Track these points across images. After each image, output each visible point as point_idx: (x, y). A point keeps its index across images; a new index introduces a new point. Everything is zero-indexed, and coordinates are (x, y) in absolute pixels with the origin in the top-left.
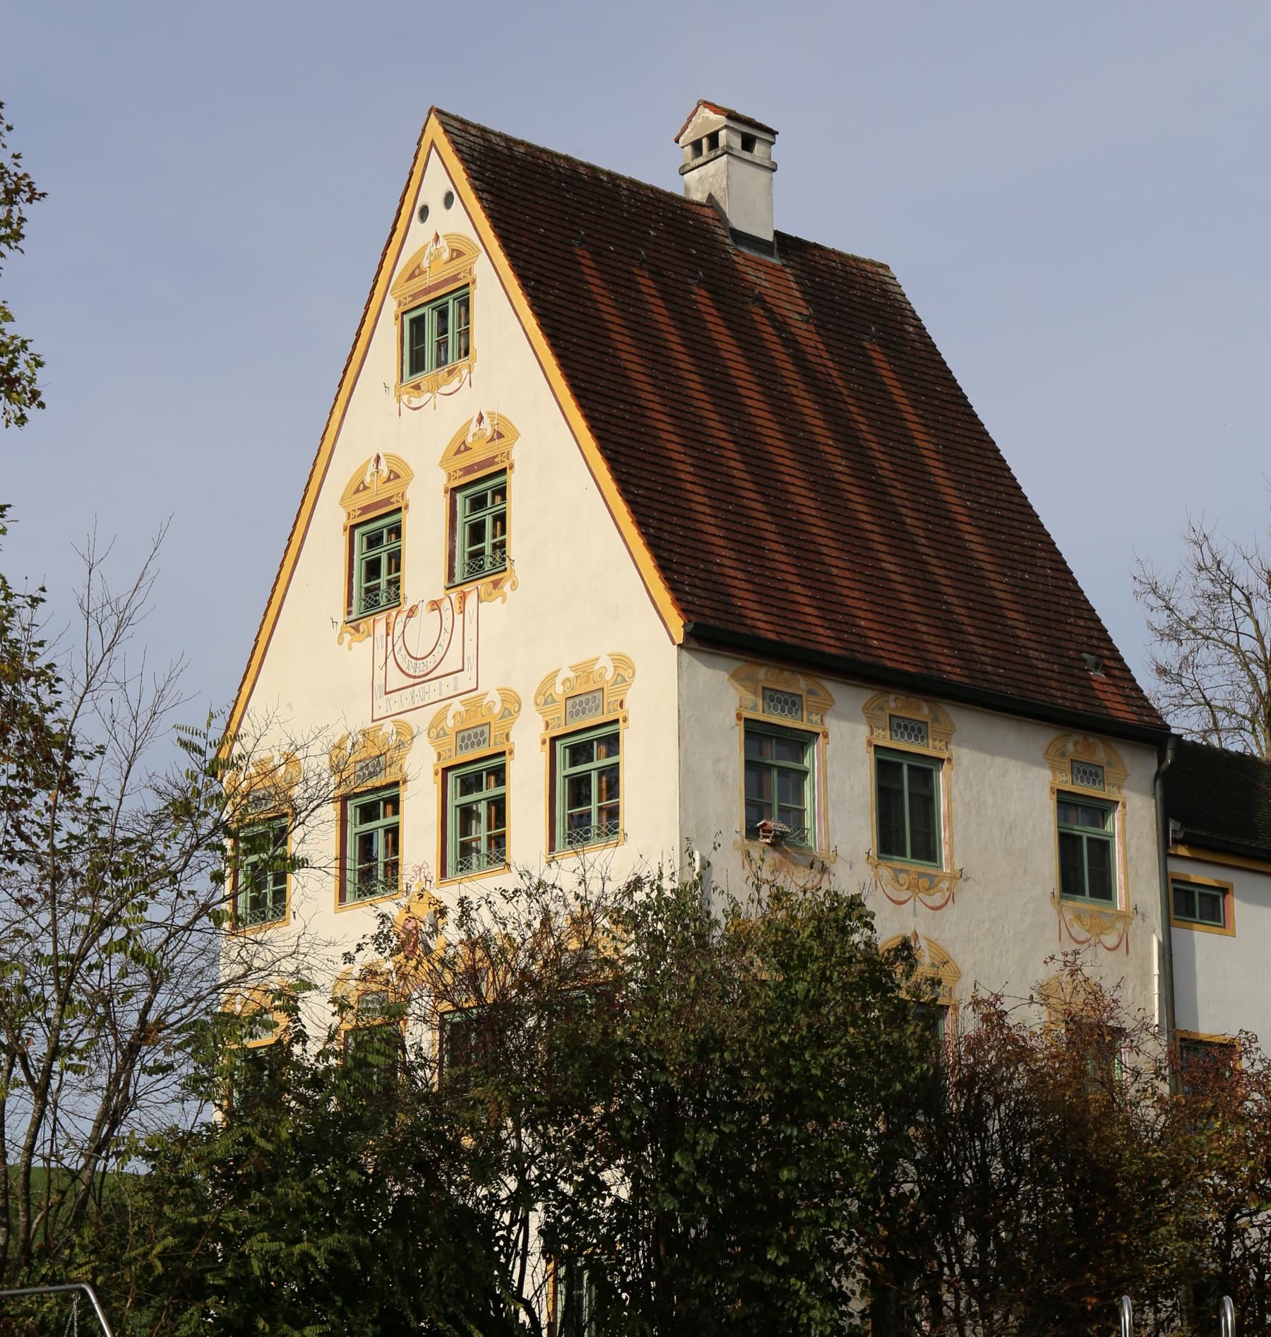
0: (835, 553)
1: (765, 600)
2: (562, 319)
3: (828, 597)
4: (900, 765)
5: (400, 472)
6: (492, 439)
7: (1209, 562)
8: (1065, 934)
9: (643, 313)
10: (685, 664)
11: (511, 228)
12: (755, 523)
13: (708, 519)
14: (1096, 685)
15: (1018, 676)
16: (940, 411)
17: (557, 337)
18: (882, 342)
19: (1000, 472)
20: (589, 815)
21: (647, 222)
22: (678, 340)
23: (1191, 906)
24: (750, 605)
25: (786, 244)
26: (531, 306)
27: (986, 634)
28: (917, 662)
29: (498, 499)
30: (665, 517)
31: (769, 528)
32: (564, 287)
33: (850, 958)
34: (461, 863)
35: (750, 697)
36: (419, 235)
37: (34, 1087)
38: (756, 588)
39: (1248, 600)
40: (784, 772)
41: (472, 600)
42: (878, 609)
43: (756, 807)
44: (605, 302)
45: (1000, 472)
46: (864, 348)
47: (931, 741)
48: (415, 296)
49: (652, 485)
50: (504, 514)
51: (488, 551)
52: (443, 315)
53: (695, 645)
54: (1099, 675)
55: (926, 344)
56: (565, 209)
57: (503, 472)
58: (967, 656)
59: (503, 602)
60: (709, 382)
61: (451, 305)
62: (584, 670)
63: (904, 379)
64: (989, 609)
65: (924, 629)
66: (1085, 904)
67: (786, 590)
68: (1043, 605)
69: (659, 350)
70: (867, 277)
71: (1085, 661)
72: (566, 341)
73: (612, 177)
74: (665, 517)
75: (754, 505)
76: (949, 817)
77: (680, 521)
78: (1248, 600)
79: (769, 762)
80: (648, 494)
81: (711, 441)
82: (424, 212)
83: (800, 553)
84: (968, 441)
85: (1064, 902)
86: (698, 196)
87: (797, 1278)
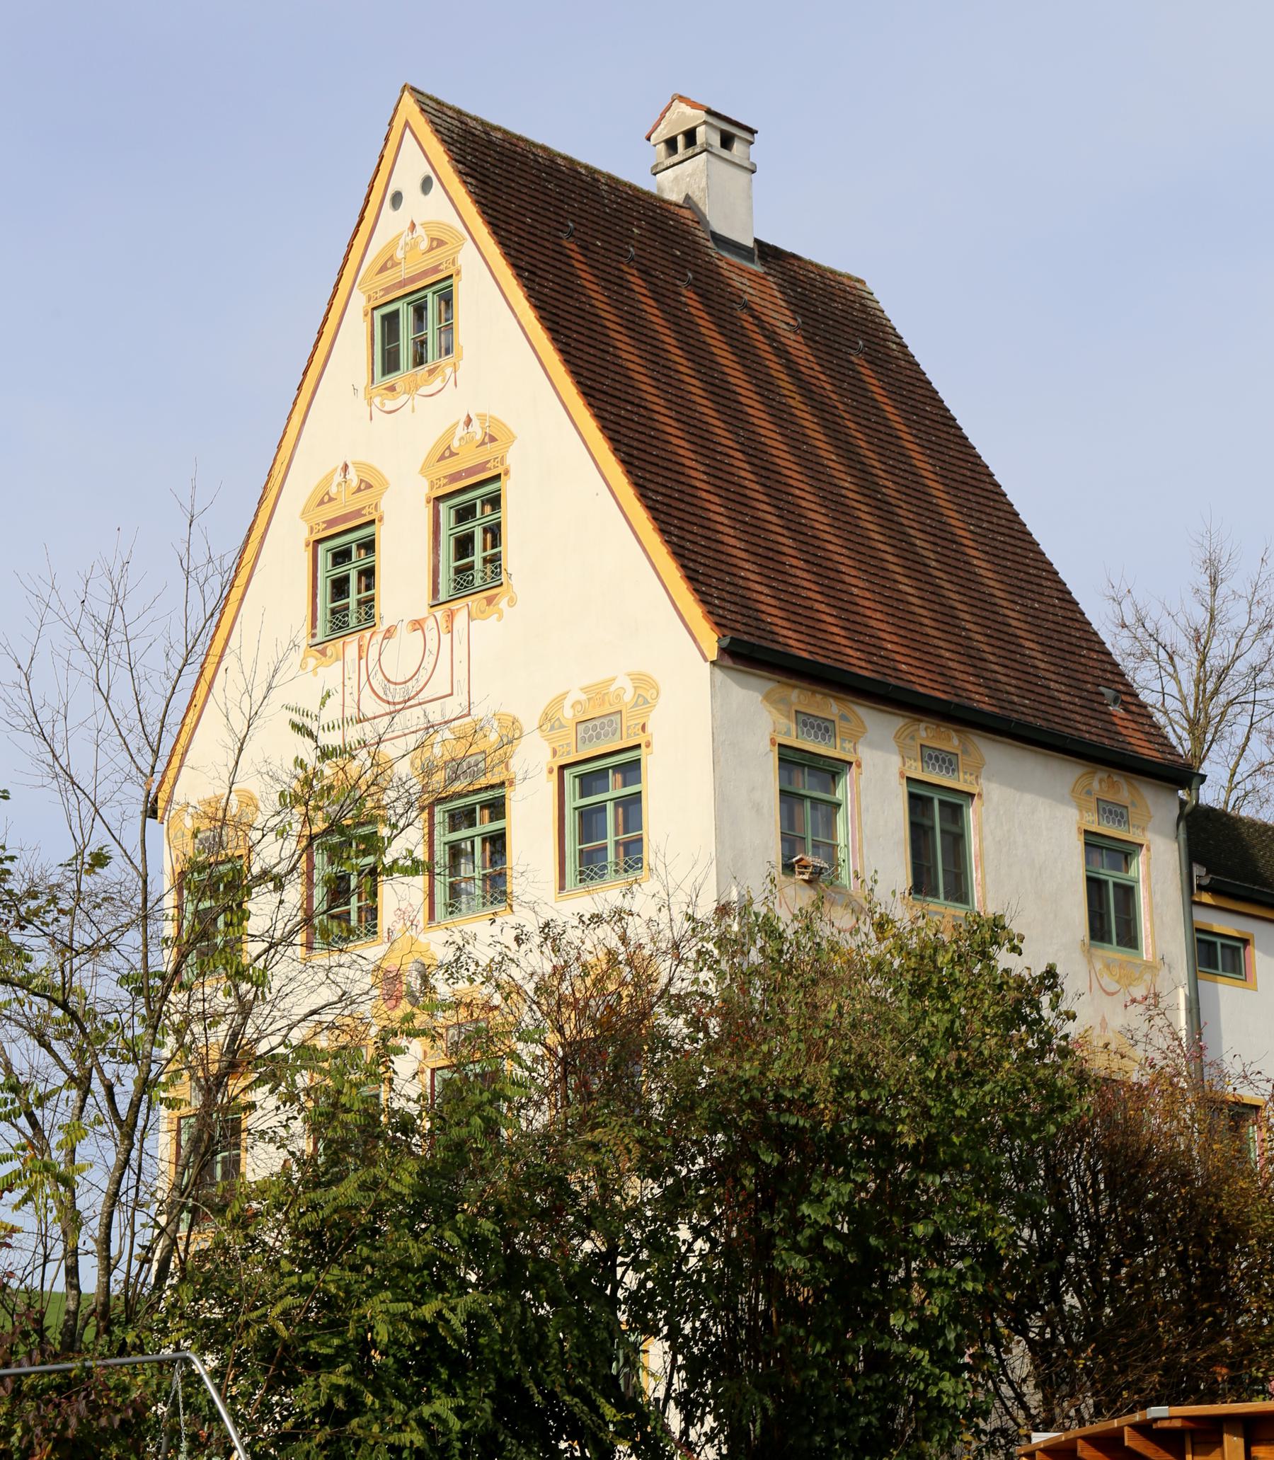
0: (853, 572)
1: (793, 617)
2: (560, 312)
3: (853, 617)
4: (931, 799)
5: (372, 482)
6: (483, 443)
7: (1130, 619)
8: (1095, 985)
9: (638, 313)
10: (718, 684)
11: (499, 215)
12: (773, 537)
13: (727, 530)
14: (1117, 721)
15: (1043, 707)
16: (932, 431)
17: (557, 332)
18: (869, 358)
19: (997, 497)
20: (605, 848)
21: (630, 219)
22: (674, 342)
23: (1215, 956)
24: (779, 622)
25: (766, 252)
26: (529, 297)
27: (1008, 663)
28: (948, 689)
29: (488, 509)
30: (686, 526)
31: (787, 543)
32: (557, 280)
33: (1002, 984)
34: (451, 905)
35: (783, 720)
36: (391, 224)
37: (120, 1123)
38: (782, 605)
39: (1171, 658)
40: (815, 801)
41: (461, 620)
42: (902, 632)
43: (791, 841)
44: (599, 299)
45: (997, 497)
46: (852, 362)
47: (961, 775)
48: (387, 290)
49: (669, 492)
50: (499, 525)
51: (478, 565)
52: (420, 311)
53: (728, 662)
54: (1116, 710)
55: (910, 362)
56: (548, 199)
57: (497, 478)
58: (991, 684)
59: (500, 619)
60: (710, 388)
61: (429, 299)
62: (597, 692)
63: (894, 396)
64: (1006, 638)
65: (948, 654)
66: (1113, 952)
67: (811, 608)
68: (1055, 636)
69: (657, 351)
70: (845, 291)
71: (1102, 694)
72: (566, 336)
73: (592, 171)
74: (686, 526)
75: (769, 517)
76: (981, 856)
77: (701, 531)
78: (1171, 658)
79: (802, 792)
80: (667, 500)
81: (720, 449)
82: (397, 199)
83: (820, 571)
84: (963, 464)
85: (1093, 950)
86: (675, 196)
87: (918, 1347)
